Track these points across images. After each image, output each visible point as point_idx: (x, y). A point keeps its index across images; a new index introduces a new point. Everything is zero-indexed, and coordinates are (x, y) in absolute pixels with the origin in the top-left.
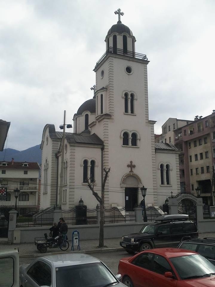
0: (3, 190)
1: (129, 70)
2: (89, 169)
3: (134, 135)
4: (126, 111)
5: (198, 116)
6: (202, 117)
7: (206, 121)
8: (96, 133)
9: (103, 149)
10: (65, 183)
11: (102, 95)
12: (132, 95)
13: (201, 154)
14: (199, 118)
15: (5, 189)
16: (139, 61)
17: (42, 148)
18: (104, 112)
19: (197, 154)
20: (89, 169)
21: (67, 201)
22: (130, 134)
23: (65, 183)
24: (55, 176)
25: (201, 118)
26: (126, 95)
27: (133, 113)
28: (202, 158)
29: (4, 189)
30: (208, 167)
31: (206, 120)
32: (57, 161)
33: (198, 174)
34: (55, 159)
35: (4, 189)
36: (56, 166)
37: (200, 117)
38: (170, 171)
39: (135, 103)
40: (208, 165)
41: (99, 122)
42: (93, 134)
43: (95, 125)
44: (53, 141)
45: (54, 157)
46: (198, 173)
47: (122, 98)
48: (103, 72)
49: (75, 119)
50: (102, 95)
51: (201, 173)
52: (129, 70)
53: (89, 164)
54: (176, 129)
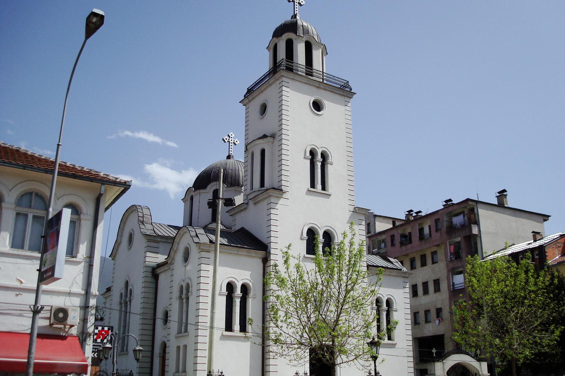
0: (105, 331)
1: (317, 106)
2: (237, 302)
3: (328, 236)
4: (313, 185)
5: (411, 211)
6: (420, 212)
7: (436, 220)
8: (246, 228)
9: (265, 260)
10: (183, 331)
11: (263, 152)
12: (324, 156)
13: (425, 284)
14: (414, 215)
15: (109, 329)
16: (335, 91)
17: (114, 257)
18: (267, 184)
19: (416, 285)
20: (237, 302)
21: (187, 370)
22: (321, 233)
23: (183, 331)
24: (150, 316)
25: (420, 214)
26: (313, 153)
27: (325, 190)
28: (426, 292)
29: (106, 329)
30: (439, 311)
31: (436, 217)
32: (155, 284)
33: (419, 324)
34: (150, 280)
35: (106, 329)
36: (152, 296)
37: (417, 213)
38: (394, 312)
39: (330, 169)
40: (439, 307)
41: (255, 204)
42: (238, 230)
43: (245, 209)
44: (149, 241)
45: (149, 275)
46: (418, 322)
47: (305, 158)
48: (264, 109)
49: (189, 199)
50: (263, 152)
51: (424, 322)
52: (317, 106)
53: (238, 292)
54: (372, 233)
